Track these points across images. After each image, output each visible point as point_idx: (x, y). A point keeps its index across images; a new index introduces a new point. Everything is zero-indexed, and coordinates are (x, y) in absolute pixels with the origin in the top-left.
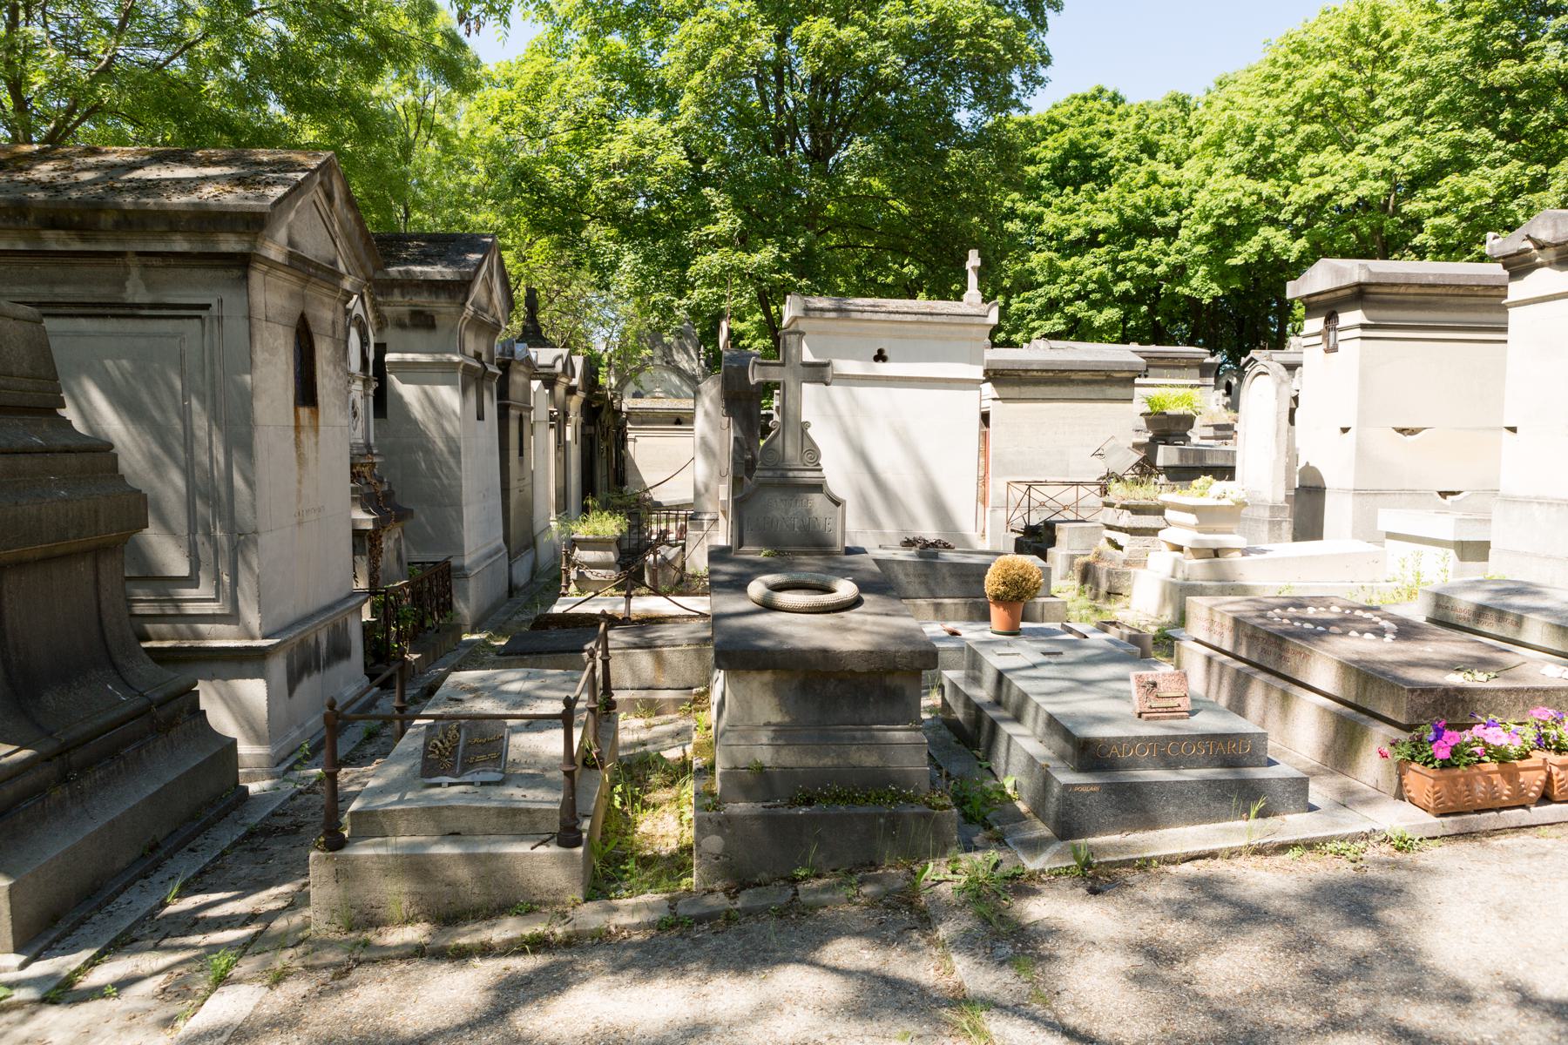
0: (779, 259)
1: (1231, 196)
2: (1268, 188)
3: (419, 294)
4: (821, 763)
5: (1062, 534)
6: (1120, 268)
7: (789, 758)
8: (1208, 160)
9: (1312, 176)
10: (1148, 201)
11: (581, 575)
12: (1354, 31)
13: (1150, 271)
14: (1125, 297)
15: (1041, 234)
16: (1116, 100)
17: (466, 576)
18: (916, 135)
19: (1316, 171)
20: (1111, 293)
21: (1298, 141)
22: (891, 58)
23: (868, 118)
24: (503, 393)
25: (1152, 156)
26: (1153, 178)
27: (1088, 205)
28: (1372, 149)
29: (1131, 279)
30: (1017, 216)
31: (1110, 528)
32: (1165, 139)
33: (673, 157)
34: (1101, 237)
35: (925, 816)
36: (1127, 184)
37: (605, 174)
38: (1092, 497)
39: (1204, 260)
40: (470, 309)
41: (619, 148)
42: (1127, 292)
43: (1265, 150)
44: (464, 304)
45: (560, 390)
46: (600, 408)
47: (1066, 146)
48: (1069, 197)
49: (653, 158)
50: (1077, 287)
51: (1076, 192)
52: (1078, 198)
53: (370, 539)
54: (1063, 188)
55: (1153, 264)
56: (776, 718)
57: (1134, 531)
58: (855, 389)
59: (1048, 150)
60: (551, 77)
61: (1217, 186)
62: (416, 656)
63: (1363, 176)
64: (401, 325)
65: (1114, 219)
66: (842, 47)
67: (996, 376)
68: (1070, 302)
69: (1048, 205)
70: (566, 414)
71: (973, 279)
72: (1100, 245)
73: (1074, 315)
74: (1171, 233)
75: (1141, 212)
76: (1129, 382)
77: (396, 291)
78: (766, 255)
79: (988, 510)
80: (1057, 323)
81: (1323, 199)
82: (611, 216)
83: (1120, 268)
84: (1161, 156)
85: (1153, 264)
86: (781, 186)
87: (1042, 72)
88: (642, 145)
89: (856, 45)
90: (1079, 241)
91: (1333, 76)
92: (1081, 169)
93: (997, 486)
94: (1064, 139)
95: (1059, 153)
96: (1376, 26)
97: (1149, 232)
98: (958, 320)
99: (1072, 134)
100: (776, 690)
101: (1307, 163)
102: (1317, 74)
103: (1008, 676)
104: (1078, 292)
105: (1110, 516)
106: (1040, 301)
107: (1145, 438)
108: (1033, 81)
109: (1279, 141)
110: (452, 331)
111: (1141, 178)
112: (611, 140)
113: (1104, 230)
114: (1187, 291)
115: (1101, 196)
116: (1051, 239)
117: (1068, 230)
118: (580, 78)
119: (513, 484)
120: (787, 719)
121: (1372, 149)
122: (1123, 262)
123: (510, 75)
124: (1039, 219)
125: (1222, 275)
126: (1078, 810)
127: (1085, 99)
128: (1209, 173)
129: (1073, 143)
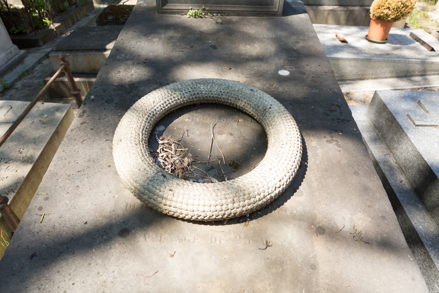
62: (57, 25)
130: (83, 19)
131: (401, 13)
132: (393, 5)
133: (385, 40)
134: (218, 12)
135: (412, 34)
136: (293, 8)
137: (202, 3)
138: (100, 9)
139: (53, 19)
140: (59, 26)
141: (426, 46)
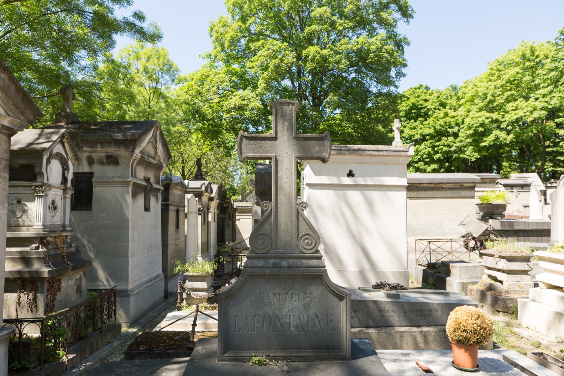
1: (480, 119)
2: (495, 116)
5: (455, 269)
6: (436, 149)
8: (468, 107)
9: (513, 110)
10: (446, 123)
12: (523, 56)
13: (449, 149)
14: (439, 161)
16: (427, 88)
17: (128, 296)
18: (355, 96)
19: (514, 108)
20: (433, 158)
21: (505, 97)
22: (343, 61)
25: (444, 107)
26: (446, 115)
27: (422, 126)
28: (537, 99)
32: (448, 101)
33: (258, 104)
36: (437, 117)
37: (228, 112)
39: (470, 144)
41: (234, 101)
43: (491, 102)
45: (205, 199)
47: (411, 105)
48: (413, 123)
49: (247, 105)
50: (419, 157)
51: (415, 121)
52: (417, 124)
53: (49, 282)
54: (410, 120)
55: (450, 147)
57: (509, 272)
60: (208, 76)
61: (474, 116)
62: (71, 356)
63: (535, 109)
64: (102, 163)
65: (432, 131)
68: (417, 162)
70: (208, 209)
72: (427, 140)
74: (456, 135)
75: (443, 127)
76: (472, 188)
77: (99, 146)
81: (517, 120)
83: (436, 149)
84: (448, 107)
85: (450, 147)
87: (404, 70)
88: (244, 100)
89: (329, 56)
91: (518, 73)
92: (417, 113)
94: (410, 103)
95: (408, 108)
96: (533, 53)
97: (447, 135)
98: (392, 153)
99: (413, 100)
101: (509, 106)
102: (510, 73)
104: (420, 159)
105: (489, 262)
108: (400, 74)
109: (497, 98)
110: (127, 165)
111: (442, 115)
112: (231, 99)
113: (428, 135)
114: (465, 156)
115: (426, 122)
116: (407, 139)
117: (414, 136)
119: (171, 241)
121: (537, 99)
122: (437, 146)
125: (479, 150)
127: (416, 88)
128: (469, 112)
129: (413, 104)
130: (105, 348)
131: (481, 335)
134: (283, 359)
135: (505, 358)
136: (361, 349)
137: (266, 350)
138: (127, 334)
139: (68, 349)
140: (73, 357)
141: (528, 373)
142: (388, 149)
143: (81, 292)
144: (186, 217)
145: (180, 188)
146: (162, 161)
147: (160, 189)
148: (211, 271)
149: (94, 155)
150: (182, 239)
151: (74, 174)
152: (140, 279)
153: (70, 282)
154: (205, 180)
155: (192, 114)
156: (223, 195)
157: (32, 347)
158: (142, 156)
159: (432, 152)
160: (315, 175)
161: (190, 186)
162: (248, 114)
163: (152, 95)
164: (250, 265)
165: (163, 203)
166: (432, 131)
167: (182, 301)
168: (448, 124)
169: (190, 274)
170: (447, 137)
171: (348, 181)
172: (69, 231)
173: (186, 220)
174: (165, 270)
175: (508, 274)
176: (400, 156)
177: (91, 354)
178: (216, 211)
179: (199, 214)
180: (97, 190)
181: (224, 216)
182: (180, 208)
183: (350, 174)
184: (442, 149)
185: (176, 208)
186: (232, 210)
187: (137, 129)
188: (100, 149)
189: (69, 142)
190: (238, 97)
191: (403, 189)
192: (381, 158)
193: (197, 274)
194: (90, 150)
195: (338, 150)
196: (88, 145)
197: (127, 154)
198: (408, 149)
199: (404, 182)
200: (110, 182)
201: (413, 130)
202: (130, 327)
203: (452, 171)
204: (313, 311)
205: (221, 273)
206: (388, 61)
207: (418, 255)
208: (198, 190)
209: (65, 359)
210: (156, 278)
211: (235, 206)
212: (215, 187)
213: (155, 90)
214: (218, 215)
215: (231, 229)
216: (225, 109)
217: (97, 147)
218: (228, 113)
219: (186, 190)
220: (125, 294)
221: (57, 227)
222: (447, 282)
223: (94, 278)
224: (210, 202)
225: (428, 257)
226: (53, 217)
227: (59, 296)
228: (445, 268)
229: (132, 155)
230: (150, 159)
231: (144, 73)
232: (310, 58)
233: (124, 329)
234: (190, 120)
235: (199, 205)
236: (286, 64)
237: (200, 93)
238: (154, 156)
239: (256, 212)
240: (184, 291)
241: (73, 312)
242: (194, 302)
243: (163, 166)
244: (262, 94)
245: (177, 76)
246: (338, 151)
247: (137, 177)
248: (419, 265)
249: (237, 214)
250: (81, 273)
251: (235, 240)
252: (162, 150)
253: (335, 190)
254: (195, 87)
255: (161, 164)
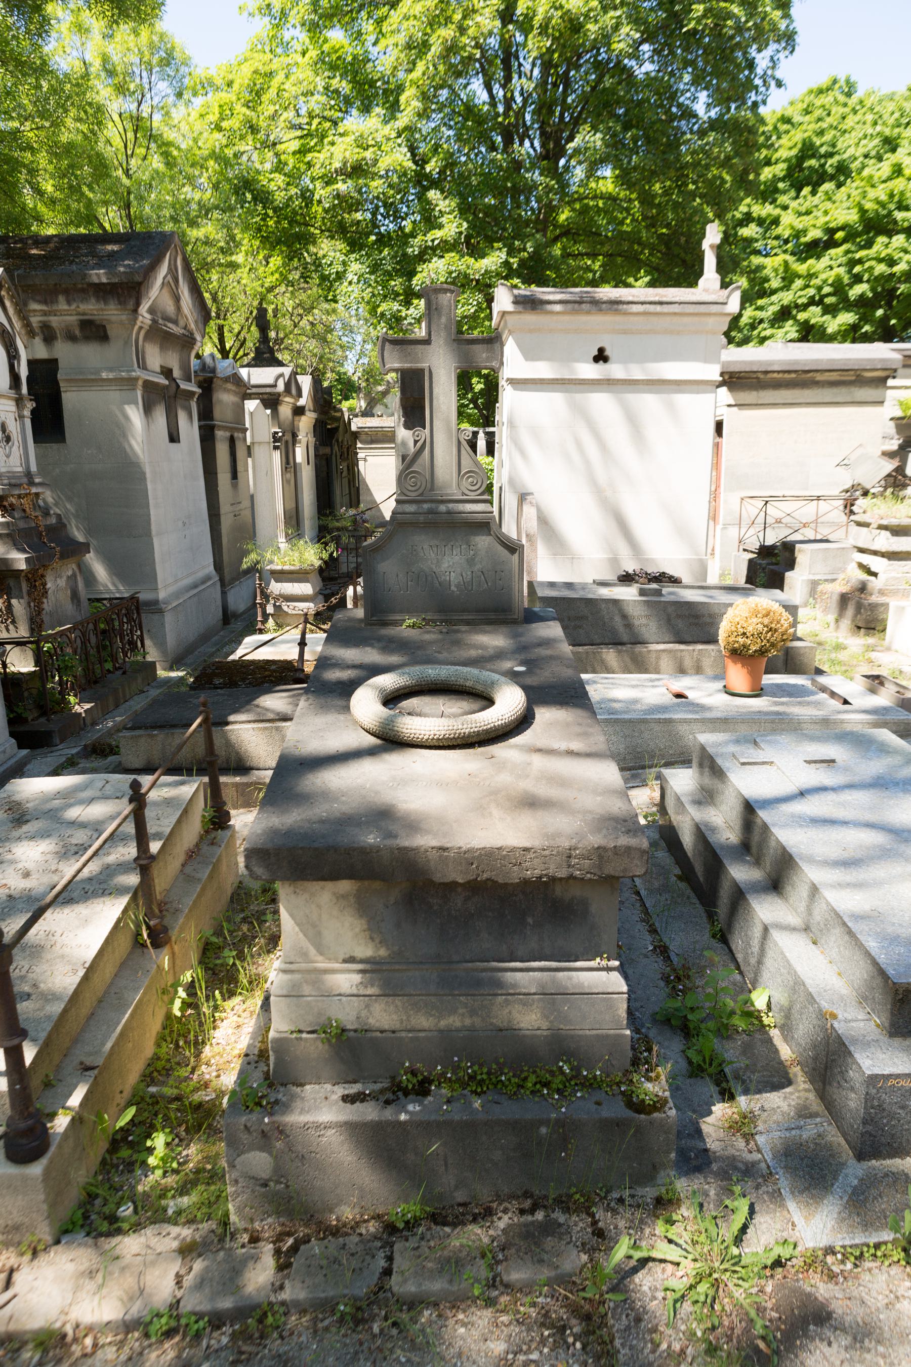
0: (506, 264)
3: (84, 300)
4: (443, 1023)
5: (803, 555)
7: (383, 1016)
10: (891, 196)
11: (278, 608)
14: (862, 303)
15: (777, 238)
17: (161, 612)
22: (625, 30)
23: (598, 106)
24: (206, 414)
26: (898, 171)
27: (828, 205)
29: (868, 281)
30: (753, 220)
31: (862, 551)
33: (397, 158)
34: (840, 235)
35: (619, 1124)
36: (871, 177)
37: (329, 181)
38: (834, 511)
40: (144, 315)
41: (339, 152)
42: (862, 296)
44: (135, 311)
45: (285, 410)
46: (336, 429)
49: (376, 161)
50: (811, 292)
51: (814, 193)
52: (816, 200)
53: (28, 580)
54: (799, 190)
55: (891, 262)
56: (365, 950)
58: (578, 396)
59: (786, 148)
60: (271, 75)
62: (87, 706)
64: (71, 338)
65: (853, 217)
66: (571, 20)
67: (734, 380)
68: (805, 307)
69: (785, 208)
70: (294, 435)
71: (710, 261)
72: (836, 244)
73: (806, 322)
77: (61, 298)
78: (494, 260)
79: (719, 527)
80: (790, 329)
82: (340, 230)
83: (857, 269)
85: (891, 262)
86: (509, 183)
89: (587, 16)
90: (815, 243)
92: (812, 171)
93: (729, 501)
94: (798, 136)
95: (794, 152)
100: (362, 907)
103: (763, 815)
104: (813, 297)
105: (863, 537)
106: (776, 308)
107: (894, 445)
110: (127, 342)
111: (885, 169)
112: (333, 144)
113: (842, 228)
116: (786, 242)
117: (805, 232)
118: (300, 77)
119: (225, 508)
120: (383, 952)
122: (860, 261)
123: (231, 77)
124: (776, 221)
126: (892, 1116)
132: (750, 629)
133: (758, 691)
138: (168, 680)
139: (83, 693)
142: (683, 299)
143: (79, 601)
144: (249, 455)
145: (234, 388)
146: (193, 326)
147: (193, 393)
148: (318, 563)
149: (54, 321)
150: (246, 503)
151: (30, 363)
152: (176, 581)
153: (59, 581)
154: (280, 364)
155: (236, 193)
156: (324, 401)
157: (24, 686)
158: (153, 320)
159: (846, 280)
160: (526, 360)
161: (253, 382)
162: (377, 186)
163: (131, 135)
164: (400, 510)
165: (202, 423)
166: (853, 217)
167: (266, 617)
168: (896, 199)
169: (279, 568)
170: (890, 234)
171: (589, 370)
172: (40, 484)
173: (250, 460)
174: (218, 566)
175: (889, 559)
176: (709, 314)
177: (117, 706)
178: (312, 440)
179: (276, 448)
180: (71, 399)
181: (327, 450)
182: (236, 435)
183: (601, 357)
184: (871, 268)
185: (228, 434)
186: (348, 435)
187: (135, 254)
188: (66, 307)
189: (12, 298)
190: (350, 139)
191: (709, 388)
192: (668, 318)
193: (292, 568)
194: (44, 308)
195: (575, 302)
196: (38, 298)
197: (124, 317)
198: (728, 297)
199: (713, 373)
200: (93, 380)
201: (804, 217)
202: (171, 669)
203: (867, 338)
204: (478, 567)
205: (333, 574)
206: (740, 29)
207: (743, 531)
208: (268, 390)
209: (78, 709)
210: (204, 581)
211: (354, 428)
212: (305, 382)
213: (138, 123)
214: (316, 449)
215: (345, 481)
216: (317, 171)
217: (57, 302)
218: (328, 184)
219: (245, 391)
220: (155, 607)
221: (19, 478)
222: (787, 581)
223: (90, 579)
224: (297, 418)
225: (761, 535)
226: (8, 456)
227: (47, 605)
228: (787, 554)
229: (136, 319)
230: (170, 325)
231: (103, 74)
232: (536, 22)
233: (161, 673)
234: (231, 209)
235: (273, 425)
236: (475, 38)
237: (254, 129)
238: (173, 317)
239: (404, 444)
240: (268, 601)
241: (78, 632)
242: (288, 620)
243: (195, 339)
244: (410, 129)
245: (186, 81)
246: (576, 306)
247: (149, 368)
248: (745, 550)
249: (359, 445)
250: (74, 566)
251: (358, 503)
252: (190, 302)
253: (567, 391)
254: (240, 109)
255: (192, 334)
